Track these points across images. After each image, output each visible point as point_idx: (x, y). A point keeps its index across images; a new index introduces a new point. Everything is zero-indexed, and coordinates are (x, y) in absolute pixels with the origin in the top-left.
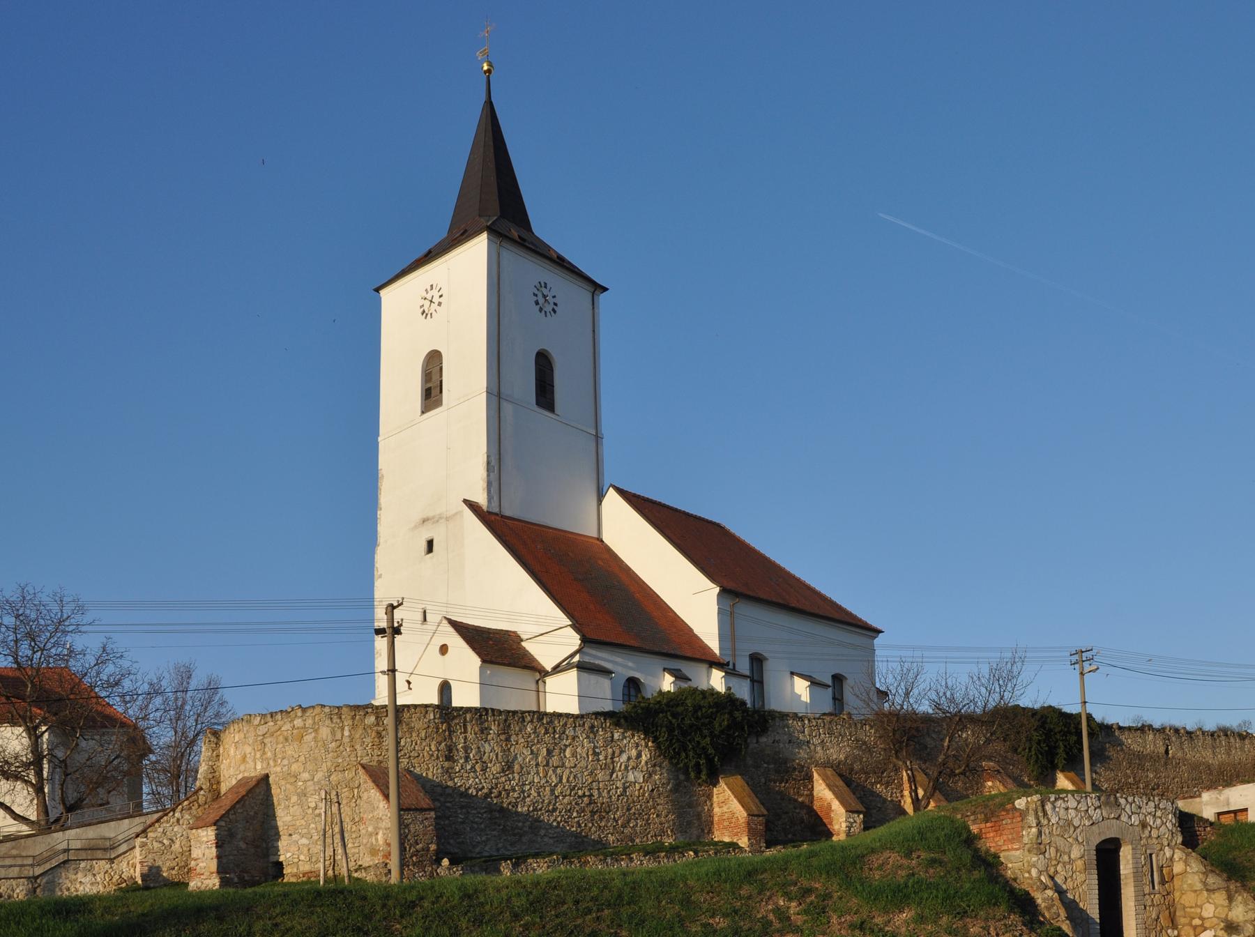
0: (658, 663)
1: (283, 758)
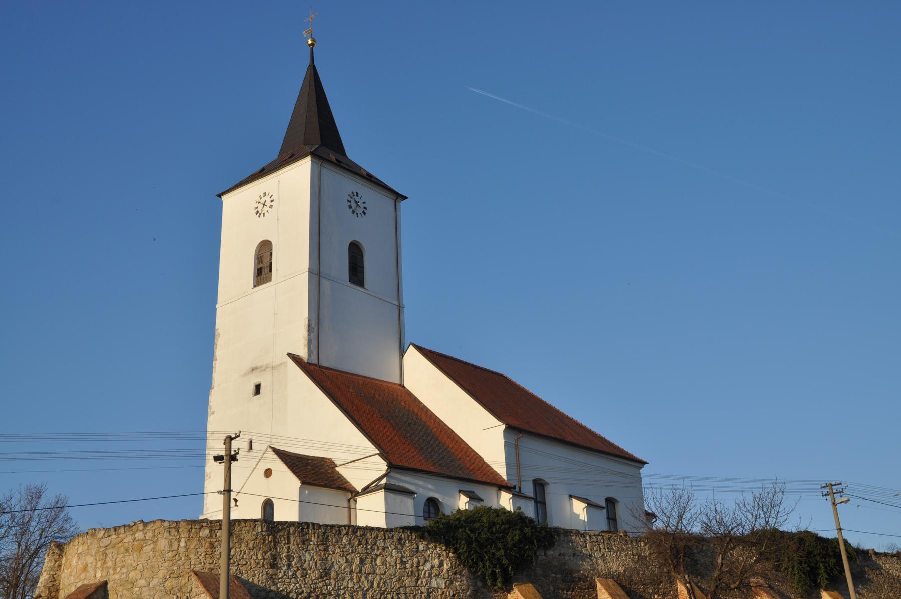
0: (453, 486)
1: (122, 567)
